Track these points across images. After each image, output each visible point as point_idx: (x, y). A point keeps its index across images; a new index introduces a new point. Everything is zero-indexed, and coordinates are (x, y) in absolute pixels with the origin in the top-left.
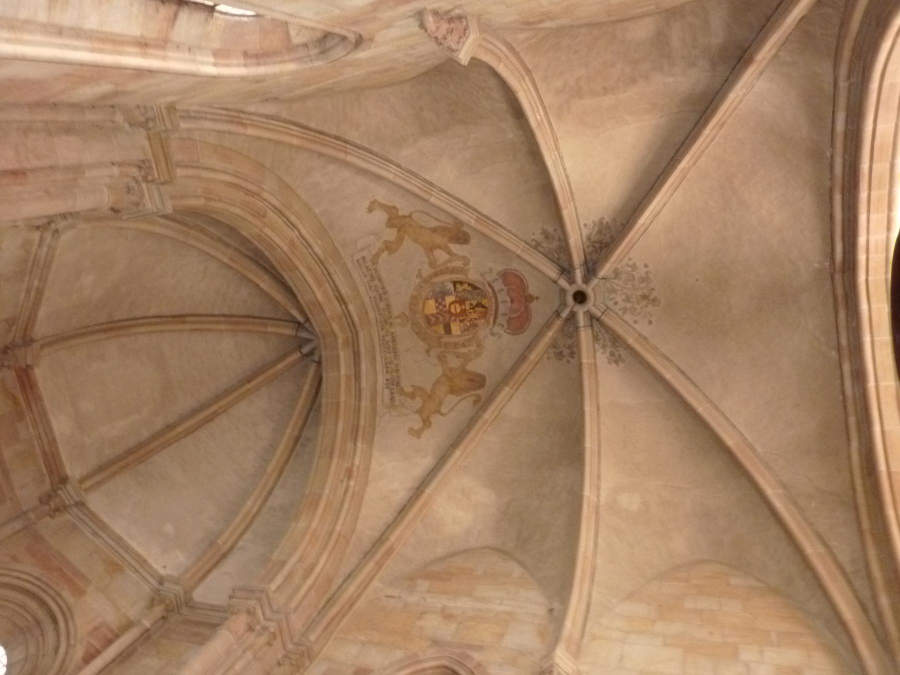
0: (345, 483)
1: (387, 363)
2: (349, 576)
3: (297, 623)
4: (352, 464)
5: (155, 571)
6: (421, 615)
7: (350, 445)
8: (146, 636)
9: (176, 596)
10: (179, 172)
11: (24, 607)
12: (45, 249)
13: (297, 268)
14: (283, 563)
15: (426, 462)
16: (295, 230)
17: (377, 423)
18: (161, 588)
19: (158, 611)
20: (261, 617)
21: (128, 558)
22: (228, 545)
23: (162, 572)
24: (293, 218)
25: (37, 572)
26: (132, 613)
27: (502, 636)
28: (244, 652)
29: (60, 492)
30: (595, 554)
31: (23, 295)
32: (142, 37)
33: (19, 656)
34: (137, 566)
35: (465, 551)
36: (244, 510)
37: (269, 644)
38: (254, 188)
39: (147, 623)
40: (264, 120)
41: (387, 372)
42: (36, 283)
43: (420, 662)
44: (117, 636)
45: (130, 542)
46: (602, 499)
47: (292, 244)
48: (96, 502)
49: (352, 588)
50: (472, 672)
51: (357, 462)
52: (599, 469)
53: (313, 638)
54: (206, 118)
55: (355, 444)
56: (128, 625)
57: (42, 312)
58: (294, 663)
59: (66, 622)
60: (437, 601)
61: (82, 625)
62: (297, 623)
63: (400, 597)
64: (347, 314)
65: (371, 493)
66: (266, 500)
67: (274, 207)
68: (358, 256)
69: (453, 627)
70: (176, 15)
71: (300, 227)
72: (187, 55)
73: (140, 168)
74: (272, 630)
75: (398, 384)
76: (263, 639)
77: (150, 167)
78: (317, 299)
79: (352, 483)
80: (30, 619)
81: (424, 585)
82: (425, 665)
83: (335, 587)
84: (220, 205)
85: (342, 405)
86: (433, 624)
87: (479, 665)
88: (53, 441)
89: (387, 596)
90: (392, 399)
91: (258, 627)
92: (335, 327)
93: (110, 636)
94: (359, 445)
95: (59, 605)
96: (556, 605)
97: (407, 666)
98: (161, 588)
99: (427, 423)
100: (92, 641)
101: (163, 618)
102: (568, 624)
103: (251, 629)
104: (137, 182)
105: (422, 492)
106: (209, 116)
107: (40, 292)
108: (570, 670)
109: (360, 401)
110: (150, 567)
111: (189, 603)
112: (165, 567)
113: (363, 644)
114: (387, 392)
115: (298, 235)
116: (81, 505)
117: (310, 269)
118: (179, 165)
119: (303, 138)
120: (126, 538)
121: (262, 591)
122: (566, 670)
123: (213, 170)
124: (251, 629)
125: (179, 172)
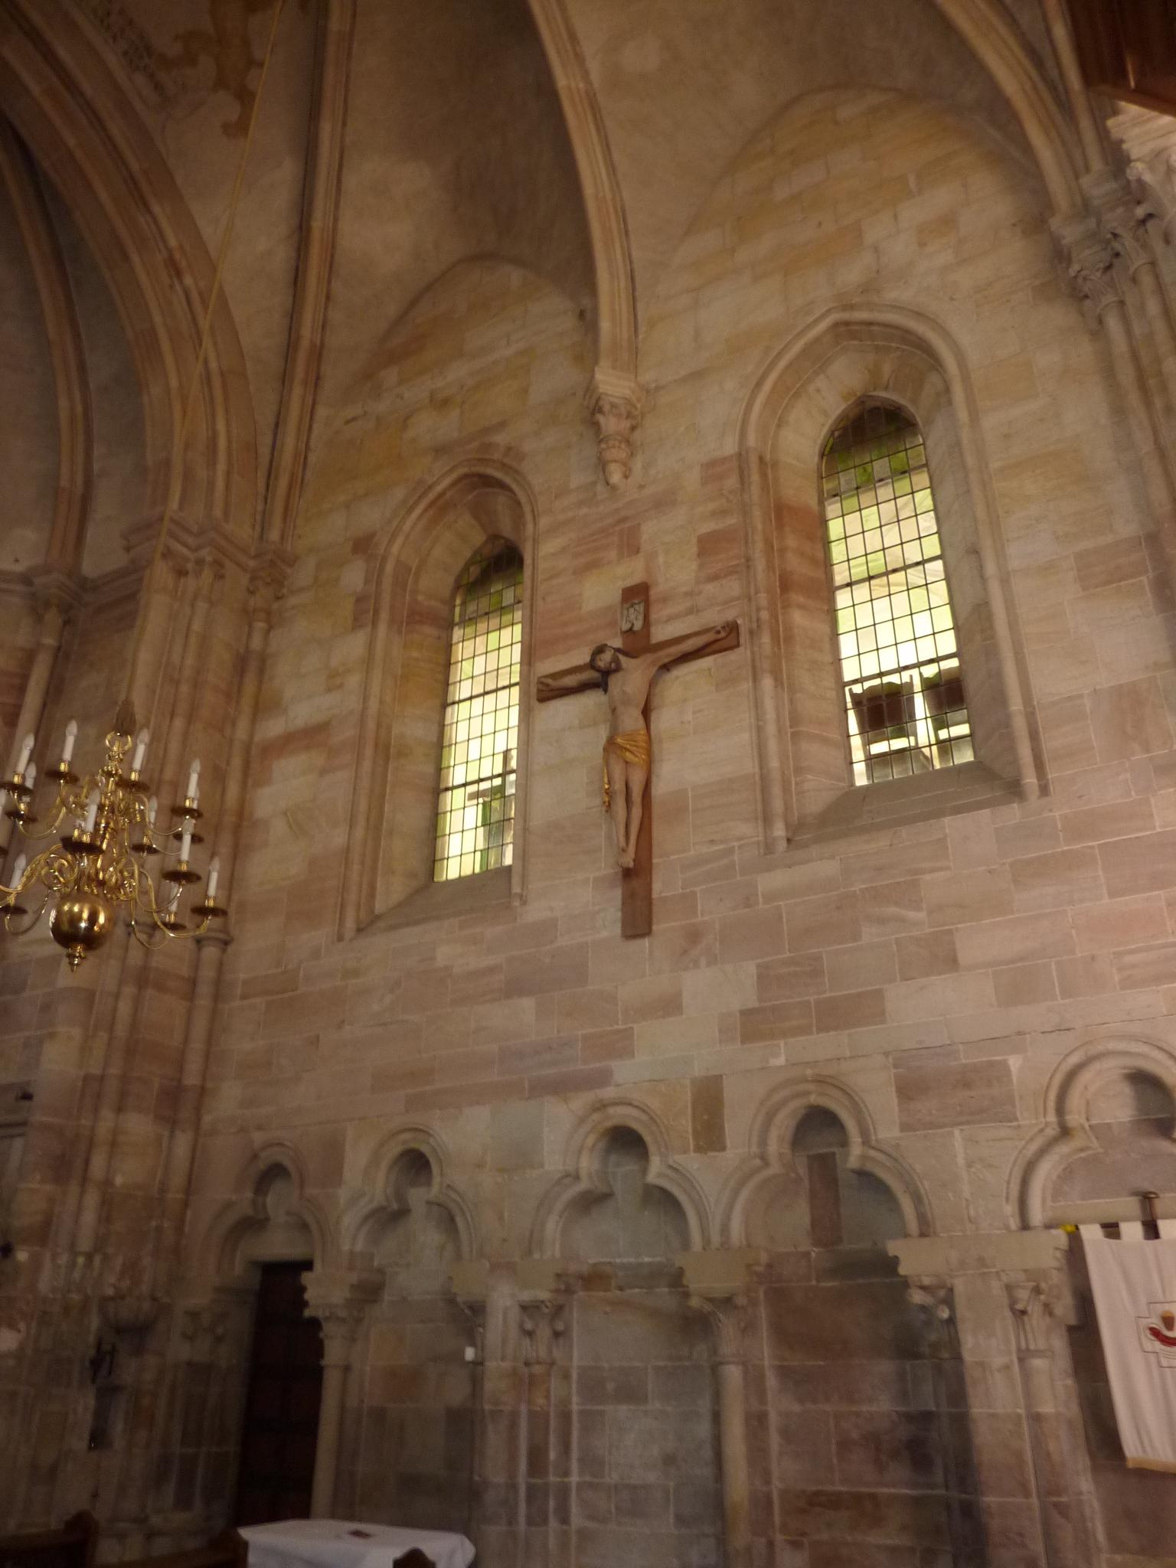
0: (178, 287)
2: (277, 425)
3: (242, 530)
4: (170, 251)
6: (405, 422)
8: (61, 655)
14: (167, 463)
15: (285, 173)
19: (53, 618)
20: (185, 551)
22: (80, 479)
23: (19, 568)
26: (23, 637)
27: (525, 391)
28: (193, 606)
30: (616, 186)
35: (428, 288)
36: (64, 416)
37: (219, 577)
39: (50, 641)
41: (115, 38)
43: (430, 487)
44: (25, 678)
46: (595, 77)
49: (290, 442)
51: (173, 242)
52: (567, 21)
53: (274, 535)
55: (149, 211)
56: (29, 658)
58: (269, 580)
62: (242, 530)
63: (365, 413)
66: (84, 383)
74: (209, 559)
76: (207, 575)
79: (188, 281)
81: (390, 375)
82: (439, 488)
83: (265, 451)
86: (429, 428)
87: (509, 449)
89: (348, 422)
90: (158, 87)
91: (190, 566)
94: (157, 209)
96: (586, 302)
97: (416, 503)
99: (245, 97)
101: (67, 623)
102: (605, 325)
103: (181, 573)
105: (309, 230)
108: (628, 392)
109: (105, 129)
111: (85, 585)
113: (347, 506)
114: (140, 79)
122: (617, 394)
124: (181, 573)
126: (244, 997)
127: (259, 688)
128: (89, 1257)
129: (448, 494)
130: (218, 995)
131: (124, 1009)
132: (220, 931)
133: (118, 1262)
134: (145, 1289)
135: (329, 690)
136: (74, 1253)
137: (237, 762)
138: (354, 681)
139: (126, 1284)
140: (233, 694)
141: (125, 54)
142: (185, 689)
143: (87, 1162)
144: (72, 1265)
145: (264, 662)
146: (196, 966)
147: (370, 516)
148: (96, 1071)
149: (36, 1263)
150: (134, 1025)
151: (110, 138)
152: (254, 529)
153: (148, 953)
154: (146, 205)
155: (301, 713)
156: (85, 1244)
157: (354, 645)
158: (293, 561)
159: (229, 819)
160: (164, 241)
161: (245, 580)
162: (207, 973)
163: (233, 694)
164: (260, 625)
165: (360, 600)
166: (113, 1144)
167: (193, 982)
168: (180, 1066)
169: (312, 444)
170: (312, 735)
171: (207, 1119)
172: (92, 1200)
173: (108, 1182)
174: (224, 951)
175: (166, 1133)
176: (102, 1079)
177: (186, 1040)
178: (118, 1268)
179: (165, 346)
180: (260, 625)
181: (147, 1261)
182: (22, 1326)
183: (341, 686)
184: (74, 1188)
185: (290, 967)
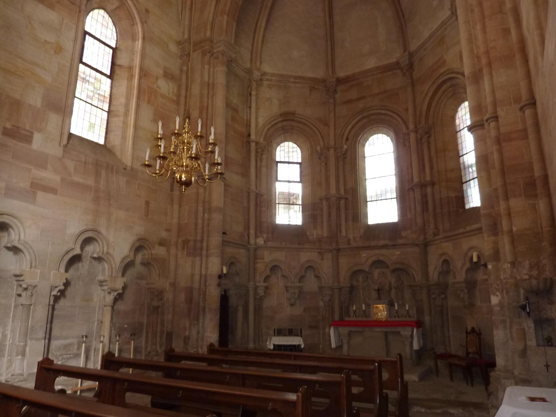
11: (444, 92)
29: (402, 66)
31: (297, 85)
32: (128, 79)
42: (292, 80)
48: (413, 47)
57: (310, 75)
70: (119, 66)
72: (135, 55)
88: (377, 68)
104: (212, 55)
107: (296, 78)
173: (511, 230)
182: (498, 293)
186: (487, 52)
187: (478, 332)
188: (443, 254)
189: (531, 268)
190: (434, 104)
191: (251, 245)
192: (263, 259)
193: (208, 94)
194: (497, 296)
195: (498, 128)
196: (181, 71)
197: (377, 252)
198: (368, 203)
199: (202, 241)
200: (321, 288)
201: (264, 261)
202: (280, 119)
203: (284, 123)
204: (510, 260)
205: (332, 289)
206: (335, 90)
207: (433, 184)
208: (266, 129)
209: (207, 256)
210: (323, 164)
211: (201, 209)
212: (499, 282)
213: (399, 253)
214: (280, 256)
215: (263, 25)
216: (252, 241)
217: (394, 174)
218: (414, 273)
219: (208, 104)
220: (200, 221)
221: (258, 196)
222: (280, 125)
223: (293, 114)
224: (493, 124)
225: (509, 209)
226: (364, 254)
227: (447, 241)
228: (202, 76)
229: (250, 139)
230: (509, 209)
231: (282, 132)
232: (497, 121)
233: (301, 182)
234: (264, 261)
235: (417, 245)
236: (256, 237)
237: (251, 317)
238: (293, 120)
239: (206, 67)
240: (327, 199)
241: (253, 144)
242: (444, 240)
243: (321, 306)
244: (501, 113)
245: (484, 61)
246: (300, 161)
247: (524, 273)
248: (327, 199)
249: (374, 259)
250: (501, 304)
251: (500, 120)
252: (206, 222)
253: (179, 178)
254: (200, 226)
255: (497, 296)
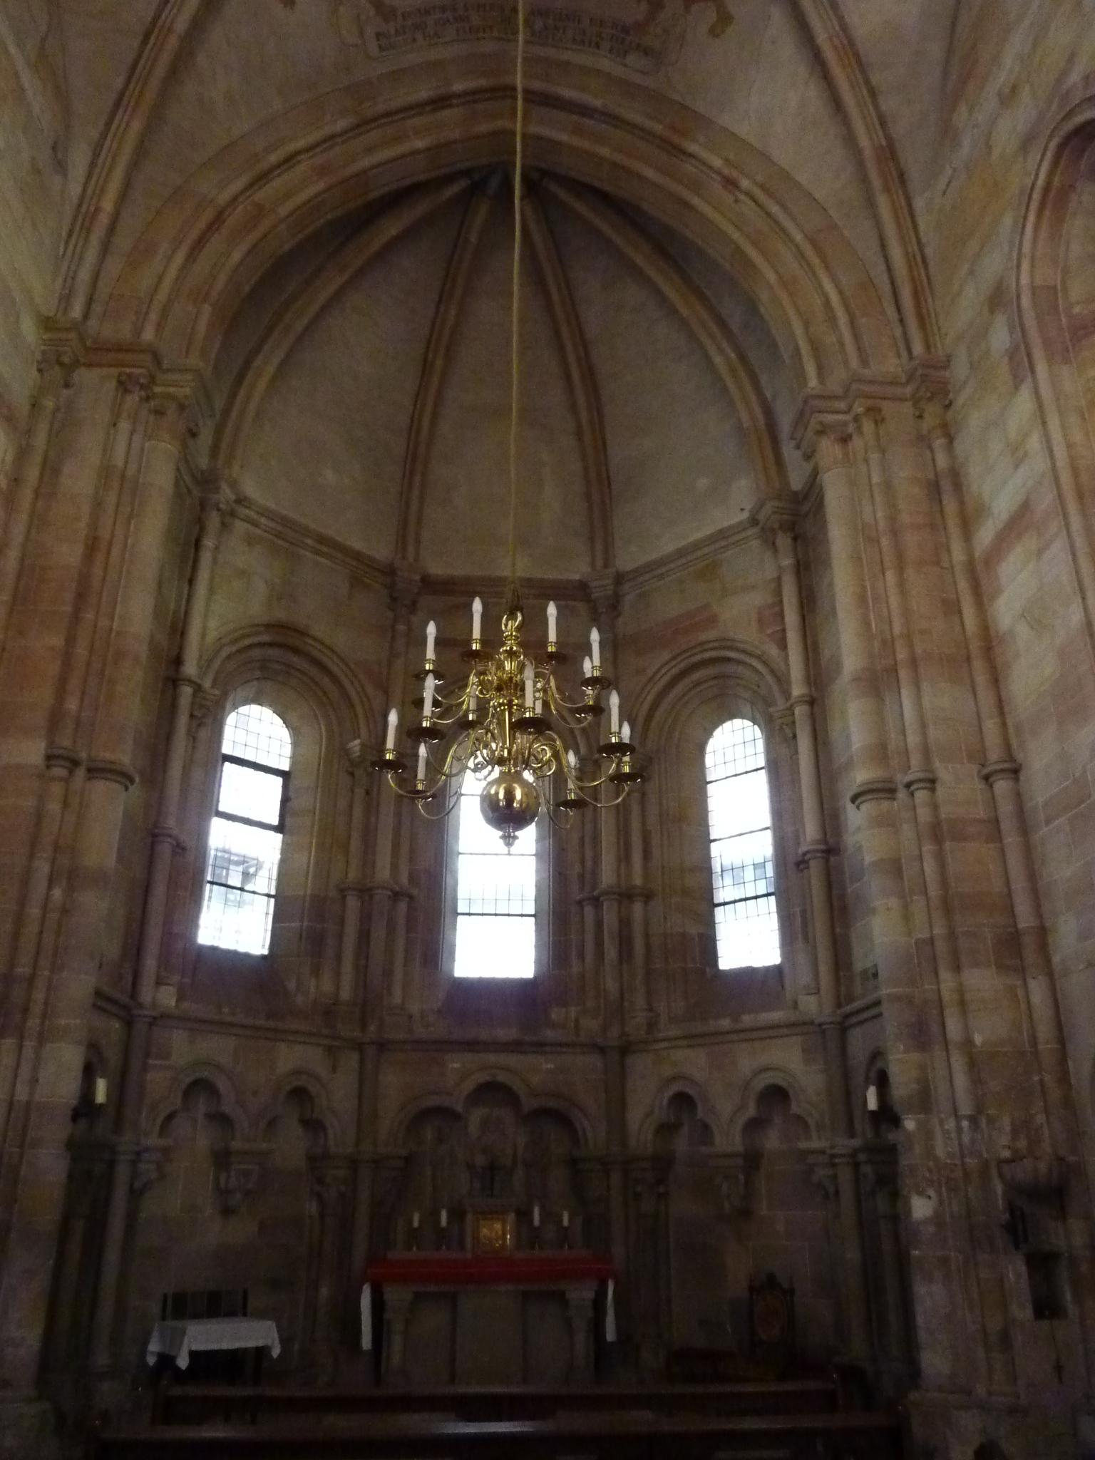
0: (742, 197)
1: (583, 42)
4: (719, 173)
5: (741, 522)
7: (689, 168)
9: (775, 513)
10: (148, 335)
11: (698, 684)
12: (263, 520)
13: (365, 172)
16: (299, 158)
17: (677, 97)
18: (761, 525)
19: (784, 541)
21: (706, 550)
23: (746, 515)
24: (274, 158)
25: (666, 655)
26: (770, 572)
33: (747, 709)
34: (723, 543)
38: (208, 215)
39: (787, 562)
40: (97, 170)
41: (598, 46)
42: (309, 541)
45: (691, 539)
47: (322, 171)
48: (628, 558)
50: (1090, 99)
51: (717, 162)
53: (918, 349)
54: (75, 272)
55: (691, 155)
57: (357, 544)
59: (737, 650)
60: (989, 102)
61: (749, 635)
63: (955, 170)
64: (472, 96)
65: (783, 155)
67: (250, 186)
68: (373, 48)
69: (1025, 94)
71: (292, 147)
73: (126, 391)
75: (626, 30)
76: (868, 426)
77: (129, 375)
78: (428, 149)
79: (745, 183)
80: (711, 683)
84: (222, 278)
85: (618, 157)
90: (647, 52)
91: (851, 428)
92: (483, 127)
93: (777, 609)
94: (693, 148)
95: (712, 649)
98: (761, 525)
100: (769, 631)
101: (795, 539)
103: (845, 440)
104: (148, 398)
106: (73, 268)
107: (322, 539)
110: (730, 527)
112: (742, 510)
113: (971, 272)
115: (307, 155)
116: (620, 579)
117: (369, 150)
118: (138, 331)
119: (134, 110)
120: (683, 543)
121: (805, 402)
123: (160, 278)
124: (845, 440)
125: (148, 335)
126: (1048, 822)
127: (962, 503)
128: (973, 1120)
129: (1056, 181)
130: (1025, 829)
131: (930, 867)
132: (1005, 761)
133: (1006, 1123)
134: (1046, 1146)
135: (1017, 466)
136: (958, 1118)
137: (963, 585)
138: (1034, 442)
139: (1022, 1144)
140: (935, 524)
141: (611, 51)
142: (885, 541)
143: (943, 1025)
144: (959, 1130)
145: (956, 477)
146: (993, 802)
147: (993, 265)
148: (926, 935)
149: (929, 1135)
150: (944, 883)
151: (634, 126)
152: (899, 356)
153: (935, 807)
154: (684, 152)
155: (1002, 505)
156: (966, 1108)
157: (1023, 403)
158: (947, 363)
159: (975, 646)
160: (710, 168)
161: (907, 408)
162: (1006, 809)
163: (935, 524)
164: (939, 443)
165: (1012, 354)
166: (962, 1003)
167: (996, 821)
168: (1010, 910)
169: (924, 240)
170: (1020, 521)
171: (1056, 959)
172: (959, 1063)
173: (969, 1042)
174: (1017, 780)
175: (1019, 983)
176: (931, 941)
177: (1008, 883)
178: (1008, 1128)
179: (752, 253)
180: (939, 443)
181: (1040, 1119)
182: (931, 1192)
183: (1026, 454)
184: (938, 1052)
185: (1077, 775)
186: (908, 637)
187: (786, 1285)
188: (674, 1079)
189: (1015, 1132)
190: (665, 706)
191: (141, 1006)
192: (167, 1056)
193: (118, 505)
194: (930, 1197)
195: (935, 807)
196: (34, 405)
197: (492, 1058)
198: (460, 918)
199: (31, 980)
200: (316, 1161)
201: (167, 1063)
202: (266, 638)
203: (272, 652)
204: (969, 1113)
205: (354, 1163)
206: (414, 603)
207: (648, 897)
208: (224, 653)
209: (42, 1039)
210: (360, 792)
211: (42, 868)
212: (931, 1164)
213: (550, 1066)
214: (218, 1048)
215: (270, 369)
216: (146, 995)
217: (534, 852)
218: (586, 1123)
219: (113, 536)
220: (34, 912)
221: (179, 849)
222: (256, 653)
223: (303, 633)
224: (921, 795)
225: (961, 991)
226: (455, 1063)
227: (689, 1046)
228: (107, 449)
229: (177, 671)
230: (961, 991)
231: (258, 674)
232: (933, 790)
233: (279, 829)
234: (167, 1063)
235: (602, 1050)
236: (159, 982)
237: (112, 1255)
238: (296, 651)
239: (124, 425)
240: (365, 892)
241: (187, 691)
242: (685, 1043)
243: (310, 1217)
244: (944, 773)
245: (902, 654)
246: (285, 766)
247: (1002, 1143)
248: (365, 892)
249: (482, 1077)
250: (937, 1219)
251: (940, 791)
252: (54, 916)
253: (505, 797)
254: (31, 929)
255: (930, 1197)
